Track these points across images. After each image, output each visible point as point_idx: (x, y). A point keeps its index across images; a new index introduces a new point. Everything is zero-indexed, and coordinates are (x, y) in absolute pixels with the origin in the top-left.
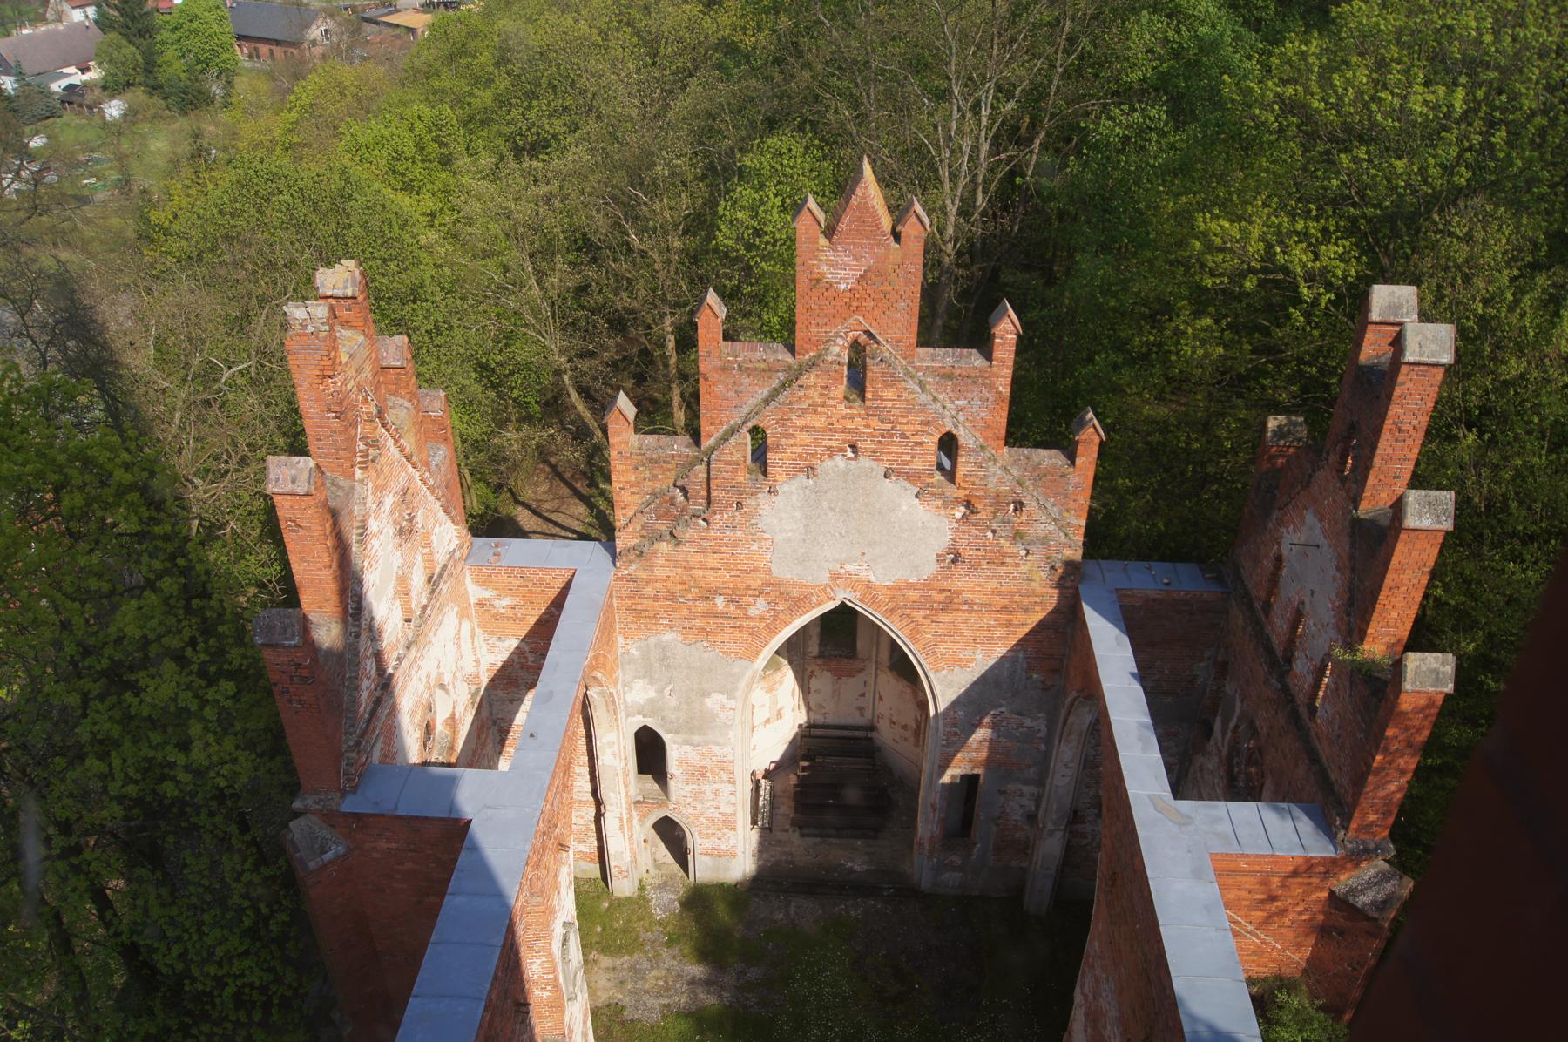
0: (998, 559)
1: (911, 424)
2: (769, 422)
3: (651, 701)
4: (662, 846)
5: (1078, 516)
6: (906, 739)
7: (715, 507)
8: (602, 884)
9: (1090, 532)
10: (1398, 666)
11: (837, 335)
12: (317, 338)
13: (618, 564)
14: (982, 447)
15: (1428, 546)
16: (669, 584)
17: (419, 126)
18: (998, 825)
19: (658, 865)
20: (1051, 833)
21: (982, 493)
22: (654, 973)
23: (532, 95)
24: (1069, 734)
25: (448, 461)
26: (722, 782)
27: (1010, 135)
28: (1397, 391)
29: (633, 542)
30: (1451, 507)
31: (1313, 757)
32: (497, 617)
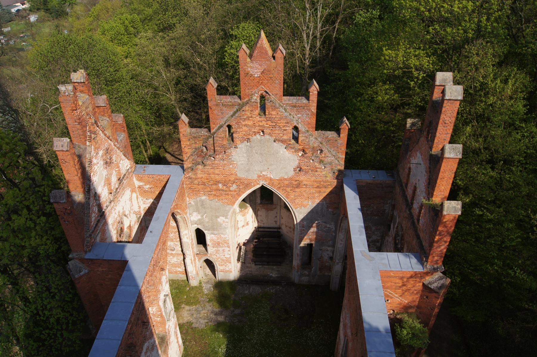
0: (315, 170)
1: (282, 123)
2: (233, 123)
3: (199, 220)
4: (208, 269)
5: (342, 155)
6: (291, 232)
7: (217, 153)
8: (187, 282)
9: (346, 162)
10: (442, 205)
11: (255, 93)
12: (69, 97)
13: (185, 173)
14: (308, 131)
15: (453, 164)
16: (203, 179)
17: (126, 22)
18: (320, 261)
19: (206, 275)
20: (338, 263)
21: (308, 147)
22: (203, 311)
23: (166, 10)
24: (342, 230)
25: (125, 138)
26: (225, 247)
27: (329, 20)
28: (443, 109)
29: (190, 165)
30: (461, 150)
31: (418, 237)
32: (145, 192)
